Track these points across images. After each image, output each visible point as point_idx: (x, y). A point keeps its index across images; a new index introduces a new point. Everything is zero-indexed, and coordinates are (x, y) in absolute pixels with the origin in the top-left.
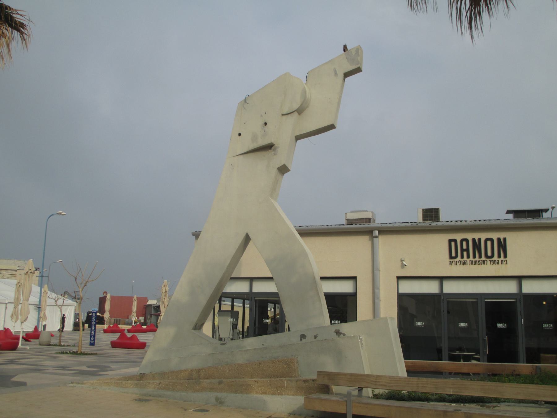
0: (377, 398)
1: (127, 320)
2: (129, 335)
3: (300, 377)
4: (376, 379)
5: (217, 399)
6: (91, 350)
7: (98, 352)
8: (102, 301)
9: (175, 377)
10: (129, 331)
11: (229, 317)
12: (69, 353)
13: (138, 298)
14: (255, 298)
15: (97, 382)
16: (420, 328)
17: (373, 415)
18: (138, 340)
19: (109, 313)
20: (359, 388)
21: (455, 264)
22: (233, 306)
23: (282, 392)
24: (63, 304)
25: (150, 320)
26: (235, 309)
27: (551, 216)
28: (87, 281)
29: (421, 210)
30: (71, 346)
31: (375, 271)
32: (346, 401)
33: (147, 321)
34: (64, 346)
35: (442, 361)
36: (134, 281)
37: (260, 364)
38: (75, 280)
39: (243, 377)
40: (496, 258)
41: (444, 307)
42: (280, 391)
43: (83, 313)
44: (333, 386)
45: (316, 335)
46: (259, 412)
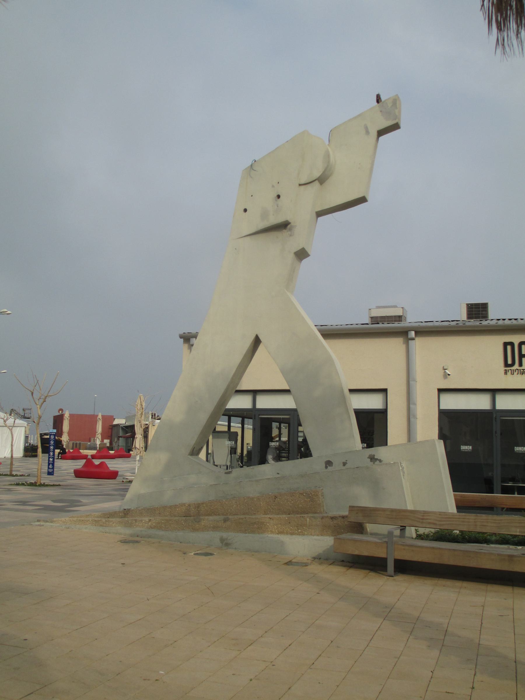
0: (422, 539)
1: (89, 444)
2: (97, 462)
3: (326, 513)
4: (423, 516)
5: (222, 540)
6: (50, 481)
7: (61, 483)
8: (58, 421)
9: (168, 514)
10: (93, 457)
11: (226, 440)
12: (26, 484)
13: (71, 416)
14: (259, 415)
15: (70, 520)
16: (466, 453)
17: (420, 560)
18: (108, 468)
19: (68, 435)
20: (401, 526)
21: (511, 374)
22: (229, 426)
23: (304, 532)
24: (14, 424)
25: (117, 444)
26: (232, 430)
28: (47, 396)
29: (465, 306)
30: (25, 476)
31: (410, 382)
32: (387, 542)
33: (114, 444)
34: (16, 475)
35: (493, 493)
36: (96, 396)
37: (276, 497)
38: (31, 394)
39: (255, 514)
41: (497, 427)
42: (301, 530)
43: (32, 436)
44: (367, 524)
45: (345, 461)
46: (275, 556)
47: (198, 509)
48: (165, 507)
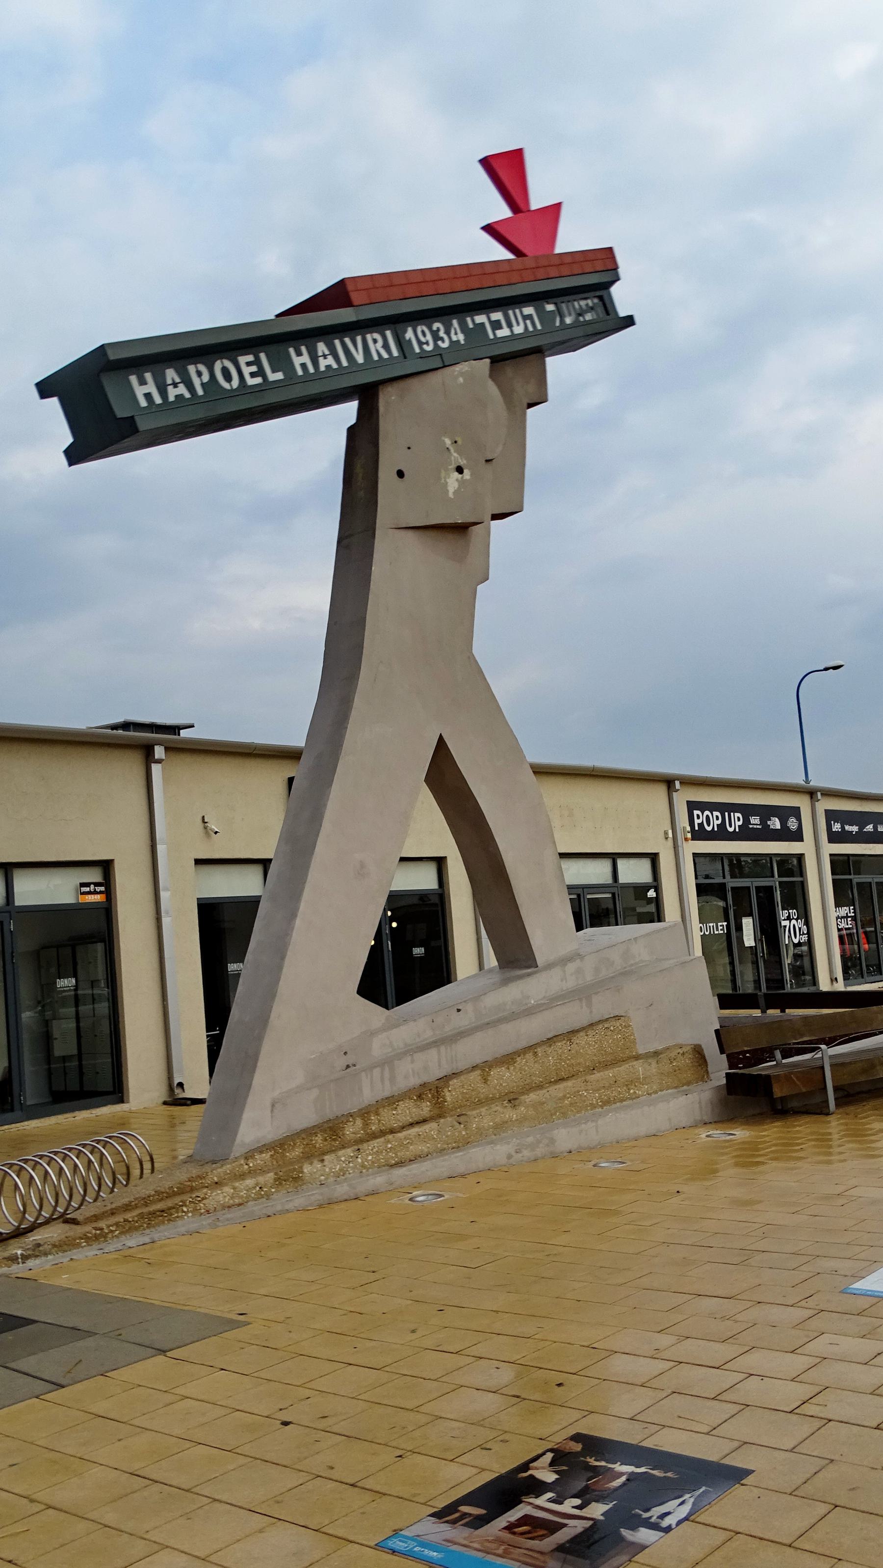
42: (633, 1089)
47: (439, 1100)
48: (366, 1115)
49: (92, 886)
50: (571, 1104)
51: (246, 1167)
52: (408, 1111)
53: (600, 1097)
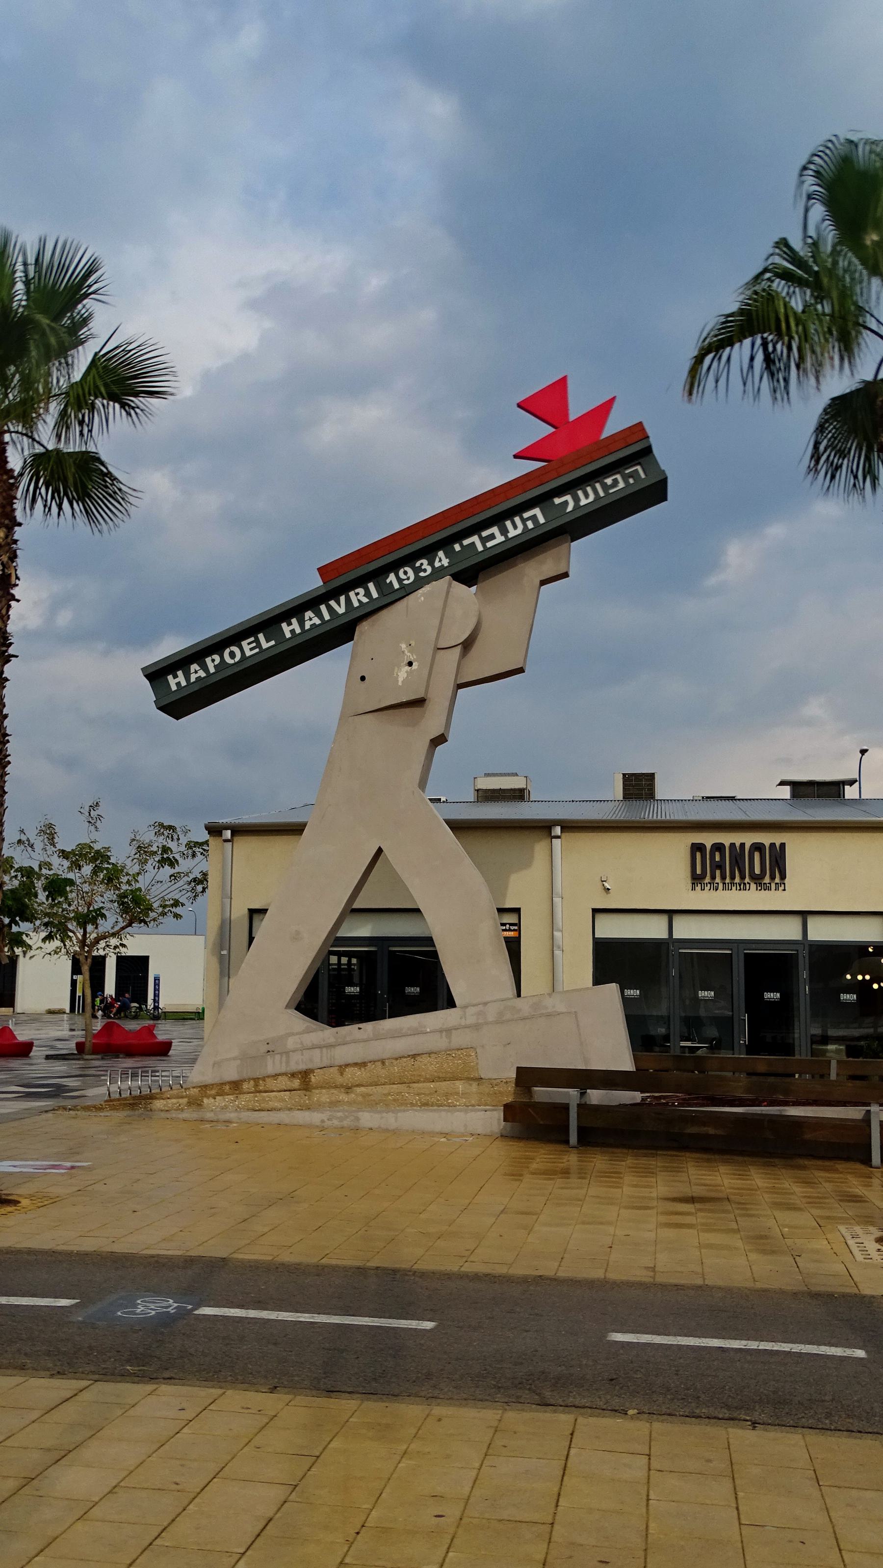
16: (352, 997)
18: (14, 1037)
27: (860, 797)
40: (767, 880)
49: (508, 926)
50: (394, 1100)
51: (185, 1093)
52: (283, 1082)
53: (419, 1100)
